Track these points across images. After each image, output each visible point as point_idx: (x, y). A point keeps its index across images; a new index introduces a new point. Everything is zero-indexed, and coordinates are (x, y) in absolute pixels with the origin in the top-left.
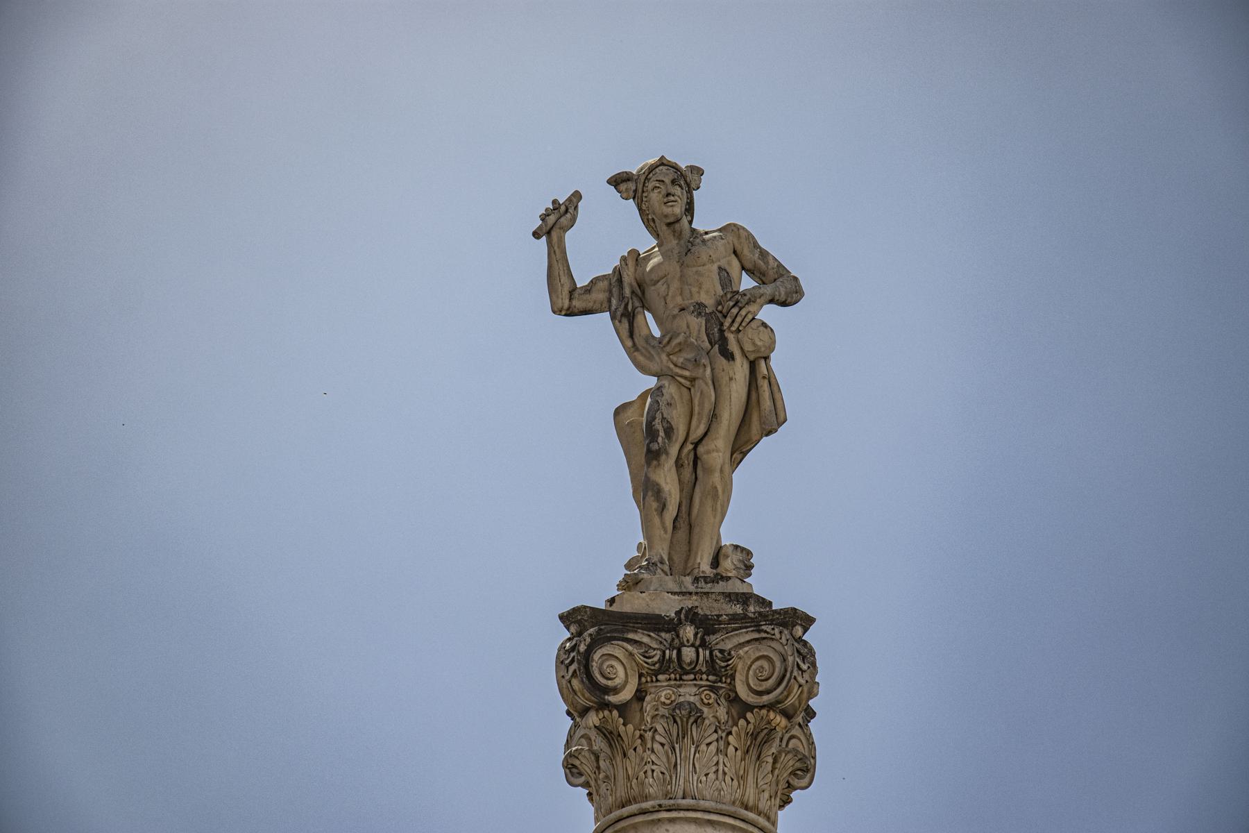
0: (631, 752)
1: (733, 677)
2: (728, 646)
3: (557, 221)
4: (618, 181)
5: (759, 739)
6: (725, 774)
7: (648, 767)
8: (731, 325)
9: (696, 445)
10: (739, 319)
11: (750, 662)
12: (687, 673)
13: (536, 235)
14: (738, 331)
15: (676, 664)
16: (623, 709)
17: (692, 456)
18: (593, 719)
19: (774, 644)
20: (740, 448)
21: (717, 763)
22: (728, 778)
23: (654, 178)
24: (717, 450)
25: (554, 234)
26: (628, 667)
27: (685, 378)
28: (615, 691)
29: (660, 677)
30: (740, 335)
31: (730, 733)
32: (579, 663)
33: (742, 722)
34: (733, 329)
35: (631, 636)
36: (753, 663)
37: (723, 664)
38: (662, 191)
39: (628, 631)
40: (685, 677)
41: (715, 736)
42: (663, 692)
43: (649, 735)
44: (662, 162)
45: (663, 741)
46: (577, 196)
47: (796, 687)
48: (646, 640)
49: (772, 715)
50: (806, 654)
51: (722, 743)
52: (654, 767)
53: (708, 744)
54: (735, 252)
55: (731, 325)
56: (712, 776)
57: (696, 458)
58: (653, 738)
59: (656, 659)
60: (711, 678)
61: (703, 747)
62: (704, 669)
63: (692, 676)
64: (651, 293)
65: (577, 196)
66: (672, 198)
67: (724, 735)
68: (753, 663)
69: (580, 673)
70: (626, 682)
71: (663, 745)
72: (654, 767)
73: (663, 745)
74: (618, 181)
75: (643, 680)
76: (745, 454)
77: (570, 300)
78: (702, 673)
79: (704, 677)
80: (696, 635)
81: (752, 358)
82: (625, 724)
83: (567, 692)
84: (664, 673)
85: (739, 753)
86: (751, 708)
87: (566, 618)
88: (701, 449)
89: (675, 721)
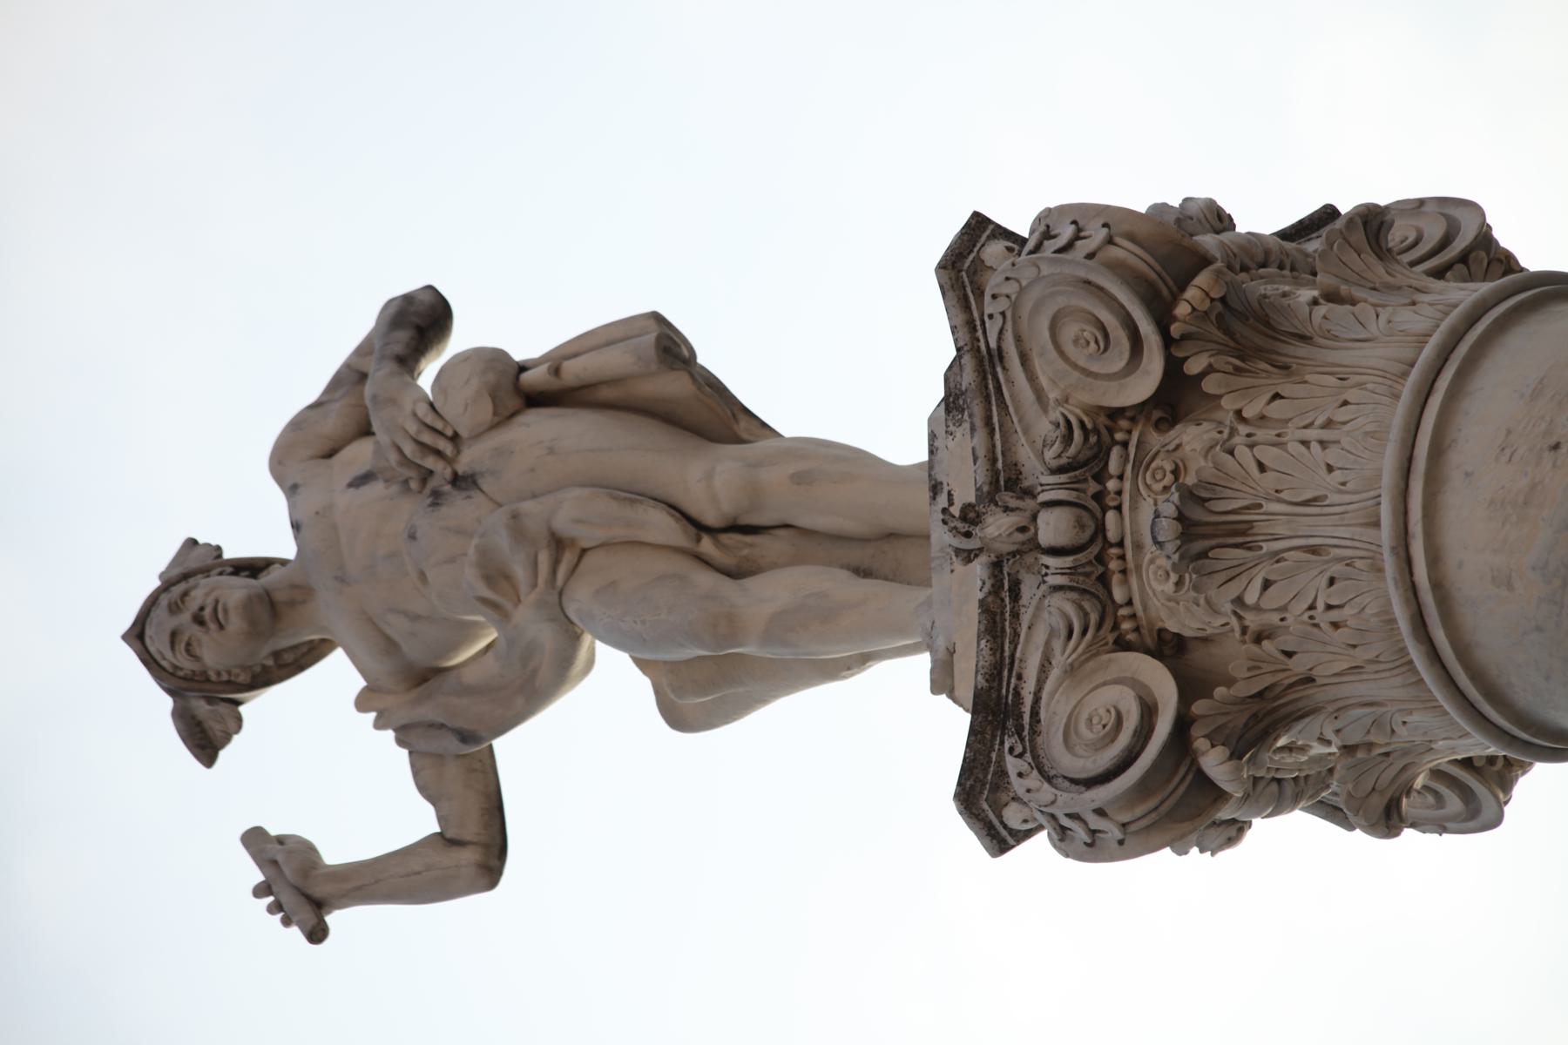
0: (1299, 666)
1: (1115, 414)
2: (1044, 427)
3: (303, 888)
4: (205, 741)
6: (1328, 424)
8: (439, 453)
9: (699, 527)
10: (427, 438)
12: (1101, 528)
13: (317, 934)
14: (455, 438)
15: (1082, 557)
16: (1191, 687)
17: (728, 539)
18: (1214, 763)
19: (1025, 312)
20: (716, 417)
22: (1341, 415)
23: (168, 654)
24: (710, 479)
25: (318, 891)
26: (1099, 679)
27: (555, 563)
28: (1149, 711)
29: (1118, 595)
31: (1238, 413)
33: (1210, 385)
34: (448, 448)
36: (1062, 353)
38: (212, 644)
40: (1112, 535)
41: (1242, 452)
42: (1156, 589)
43: (1252, 620)
45: (1257, 584)
46: (255, 840)
47: (1114, 252)
48: (1040, 636)
49: (1182, 310)
51: (1262, 434)
52: (1320, 605)
53: (1262, 467)
54: (330, 454)
55: (439, 453)
56: (1332, 456)
57: (736, 528)
58: (1257, 608)
59: (1070, 610)
60: (1113, 466)
62: (1093, 487)
63: (1111, 516)
64: (415, 652)
65: (255, 840)
66: (207, 613)
67: (1243, 429)
68: (1062, 353)
69: (1178, 795)
70: (1134, 683)
71: (1267, 584)
72: (1320, 605)
73: (1267, 584)
74: (205, 741)
77: (470, 848)
80: (1007, 509)
81: (514, 402)
87: (999, 840)
88: (710, 518)
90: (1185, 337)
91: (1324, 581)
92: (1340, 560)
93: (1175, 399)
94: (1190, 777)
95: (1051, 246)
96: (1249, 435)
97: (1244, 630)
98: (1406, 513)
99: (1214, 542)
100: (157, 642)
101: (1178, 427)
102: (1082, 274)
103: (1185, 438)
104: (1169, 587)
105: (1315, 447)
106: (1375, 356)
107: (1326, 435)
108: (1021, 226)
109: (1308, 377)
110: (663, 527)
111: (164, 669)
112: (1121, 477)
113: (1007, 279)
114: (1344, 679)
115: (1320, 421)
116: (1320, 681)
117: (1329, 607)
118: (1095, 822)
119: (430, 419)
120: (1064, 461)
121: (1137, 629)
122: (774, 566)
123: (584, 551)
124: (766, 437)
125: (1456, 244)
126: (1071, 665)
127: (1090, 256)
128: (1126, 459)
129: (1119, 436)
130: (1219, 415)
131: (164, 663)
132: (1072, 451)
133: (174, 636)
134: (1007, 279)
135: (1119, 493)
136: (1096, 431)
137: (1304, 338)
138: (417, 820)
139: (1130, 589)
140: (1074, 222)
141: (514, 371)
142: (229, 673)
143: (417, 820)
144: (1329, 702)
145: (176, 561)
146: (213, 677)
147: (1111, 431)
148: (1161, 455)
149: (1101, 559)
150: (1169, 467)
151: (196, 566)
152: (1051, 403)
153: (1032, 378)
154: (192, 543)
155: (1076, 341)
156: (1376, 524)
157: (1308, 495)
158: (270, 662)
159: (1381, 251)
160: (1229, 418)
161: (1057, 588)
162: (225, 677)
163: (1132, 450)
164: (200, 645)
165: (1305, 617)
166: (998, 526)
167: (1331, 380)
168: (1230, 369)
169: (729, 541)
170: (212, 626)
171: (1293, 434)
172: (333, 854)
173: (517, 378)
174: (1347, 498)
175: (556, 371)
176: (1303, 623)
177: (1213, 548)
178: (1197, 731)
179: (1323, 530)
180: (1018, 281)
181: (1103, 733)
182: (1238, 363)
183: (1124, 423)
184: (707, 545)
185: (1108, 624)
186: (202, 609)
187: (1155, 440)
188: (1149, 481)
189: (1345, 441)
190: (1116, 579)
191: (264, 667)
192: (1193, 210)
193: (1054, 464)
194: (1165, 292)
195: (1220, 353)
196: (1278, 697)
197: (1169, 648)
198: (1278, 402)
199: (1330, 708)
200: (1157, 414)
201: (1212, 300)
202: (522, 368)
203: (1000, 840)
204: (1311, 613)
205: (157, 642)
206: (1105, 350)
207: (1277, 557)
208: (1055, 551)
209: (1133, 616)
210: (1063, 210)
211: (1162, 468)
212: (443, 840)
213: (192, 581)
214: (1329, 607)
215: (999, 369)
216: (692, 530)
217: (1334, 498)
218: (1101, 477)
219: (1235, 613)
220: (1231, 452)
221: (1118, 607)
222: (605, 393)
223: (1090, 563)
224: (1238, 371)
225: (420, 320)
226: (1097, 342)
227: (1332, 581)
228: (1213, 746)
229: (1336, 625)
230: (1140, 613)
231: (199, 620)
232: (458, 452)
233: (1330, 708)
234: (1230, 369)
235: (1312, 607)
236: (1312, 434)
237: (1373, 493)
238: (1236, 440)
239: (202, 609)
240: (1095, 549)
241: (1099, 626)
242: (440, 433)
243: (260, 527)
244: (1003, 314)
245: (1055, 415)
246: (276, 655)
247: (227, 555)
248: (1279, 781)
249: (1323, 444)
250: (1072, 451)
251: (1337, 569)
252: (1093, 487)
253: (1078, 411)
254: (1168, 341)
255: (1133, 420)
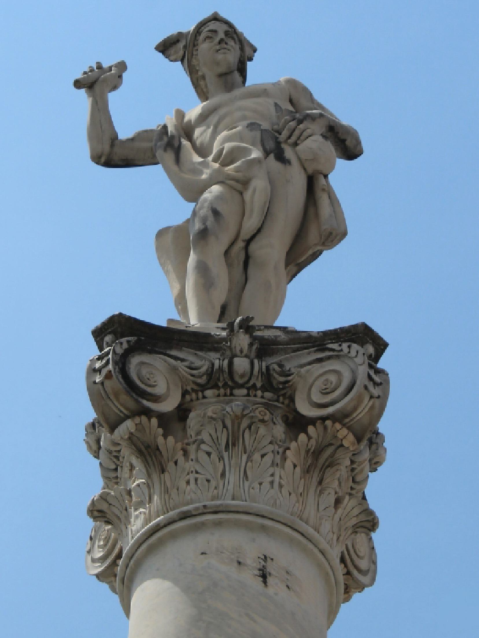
1: (292, 400)
3: (98, 83)
4: (166, 48)
5: (321, 460)
6: (281, 486)
7: (192, 477)
8: (289, 137)
9: (248, 242)
11: (314, 387)
12: (242, 386)
13: (78, 84)
16: (164, 420)
18: (129, 425)
21: (272, 475)
22: (285, 491)
23: (207, 29)
24: (272, 248)
25: (97, 87)
28: (156, 399)
30: (298, 148)
31: (288, 448)
32: (115, 363)
35: (174, 353)
36: (321, 375)
37: (282, 379)
38: (212, 52)
39: (171, 348)
40: (236, 392)
41: (271, 447)
42: (209, 407)
44: (215, 18)
46: (122, 66)
50: (379, 380)
53: (263, 456)
56: (266, 485)
58: (198, 449)
59: (204, 369)
60: (268, 395)
61: (257, 456)
62: (259, 385)
63: (244, 391)
65: (122, 66)
67: (281, 450)
71: (209, 454)
72: (197, 475)
74: (166, 48)
75: (188, 397)
76: (300, 267)
77: (113, 153)
78: (256, 390)
79: (259, 393)
80: (251, 345)
81: (310, 171)
82: (165, 436)
83: (98, 395)
84: (212, 388)
85: (298, 469)
86: (313, 421)
87: (99, 334)
88: (253, 247)
89: (225, 426)
90: (325, 428)
91: (209, 477)
92: (218, 484)
93: (297, 424)
94: (122, 415)
95: (372, 373)
96: (278, 453)
97: (188, 444)
98: (238, 512)
99: (230, 432)
100: (212, 26)
101: (284, 424)
102: (358, 382)
103: (278, 427)
104: (210, 414)
105: (270, 479)
106: (311, 511)
107: (276, 485)
108: (381, 364)
109: (303, 480)
110: (251, 224)
111: (200, 28)
112: (262, 397)
113: (357, 352)
114: (163, 485)
115: (283, 482)
116: (162, 476)
117: (196, 480)
118: (104, 372)
119: (305, 134)
120: (272, 372)
121: (192, 400)
122: (230, 273)
123: (241, 193)
124: (288, 274)
125: (353, 574)
126: (178, 369)
127: (366, 387)
128: (270, 400)
129: (281, 399)
130: (288, 440)
131: (202, 28)
132: (276, 376)
133: (215, 32)
134: (357, 352)
135: (255, 396)
136: (283, 389)
137: (320, 483)
138: (125, 131)
139: (211, 398)
140: (379, 397)
141: (325, 172)
142: (196, 55)
143: (125, 131)
144: (152, 481)
145: (248, 42)
146: (195, 48)
147: (284, 395)
148: (271, 416)
149: (225, 385)
150: (266, 418)
151: (245, 52)
152: (299, 369)
153: (310, 363)
154: (255, 51)
155: (327, 380)
156: (233, 499)
157: (249, 473)
158: (200, 73)
159: (356, 529)
160: (286, 445)
161: (213, 365)
162: (194, 53)
163: (276, 403)
164: (210, 42)
165: (192, 469)
166: (242, 340)
167: (301, 490)
168: (309, 447)
169: (243, 257)
170: (218, 47)
171: (278, 471)
172: (113, 98)
173: (321, 173)
174: (246, 489)
175: (323, 190)
176: (190, 468)
177: (227, 429)
178: (144, 419)
179: (232, 477)
180: (356, 356)
181: (145, 378)
182: (312, 451)
183: (287, 402)
184: (240, 244)
185: (195, 387)
186: (226, 43)
187: (279, 413)
188: (260, 409)
189: (272, 491)
190: (216, 392)
191: (197, 71)
192: (381, 451)
193: (271, 367)
194: (347, 420)
195: (317, 442)
196: (155, 456)
197: (182, 413)
198: (292, 466)
199: (150, 482)
200: (291, 417)
201: (342, 440)
202: (326, 176)
203: (99, 334)
204: (194, 472)
205: (212, 26)
206: (322, 393)
207: (221, 458)
208: (231, 364)
209: (198, 399)
210: (387, 382)
211: (265, 414)
212: (114, 138)
213: (238, 42)
214: (196, 480)
215: (315, 349)
216: (248, 237)
217: (247, 484)
218: (264, 389)
219: (196, 441)
220: (271, 443)
221: (202, 392)
222: (311, 211)
223: (224, 380)
224: (308, 452)
225: (347, 145)
226: (326, 389)
227: (208, 481)
228: (136, 425)
229: (188, 483)
230: (199, 402)
231: (221, 41)
232: (289, 145)
233: (150, 482)
234: (309, 447)
235: (197, 472)
236: (277, 479)
237: (247, 498)
238: (277, 447)
239: (226, 43)
240: (230, 383)
241: (195, 383)
242: (299, 138)
243: (259, 73)
244: (342, 350)
245: (293, 370)
246: (203, 77)
247: (249, 64)
248: (116, 469)
249: (272, 483)
250: (276, 376)
251: (213, 483)
252: (259, 385)
253: (294, 380)
254: (323, 419)
255: (288, 406)
